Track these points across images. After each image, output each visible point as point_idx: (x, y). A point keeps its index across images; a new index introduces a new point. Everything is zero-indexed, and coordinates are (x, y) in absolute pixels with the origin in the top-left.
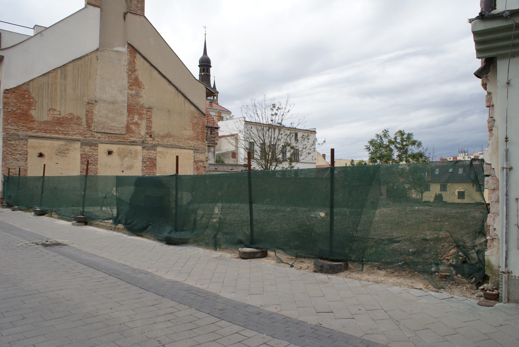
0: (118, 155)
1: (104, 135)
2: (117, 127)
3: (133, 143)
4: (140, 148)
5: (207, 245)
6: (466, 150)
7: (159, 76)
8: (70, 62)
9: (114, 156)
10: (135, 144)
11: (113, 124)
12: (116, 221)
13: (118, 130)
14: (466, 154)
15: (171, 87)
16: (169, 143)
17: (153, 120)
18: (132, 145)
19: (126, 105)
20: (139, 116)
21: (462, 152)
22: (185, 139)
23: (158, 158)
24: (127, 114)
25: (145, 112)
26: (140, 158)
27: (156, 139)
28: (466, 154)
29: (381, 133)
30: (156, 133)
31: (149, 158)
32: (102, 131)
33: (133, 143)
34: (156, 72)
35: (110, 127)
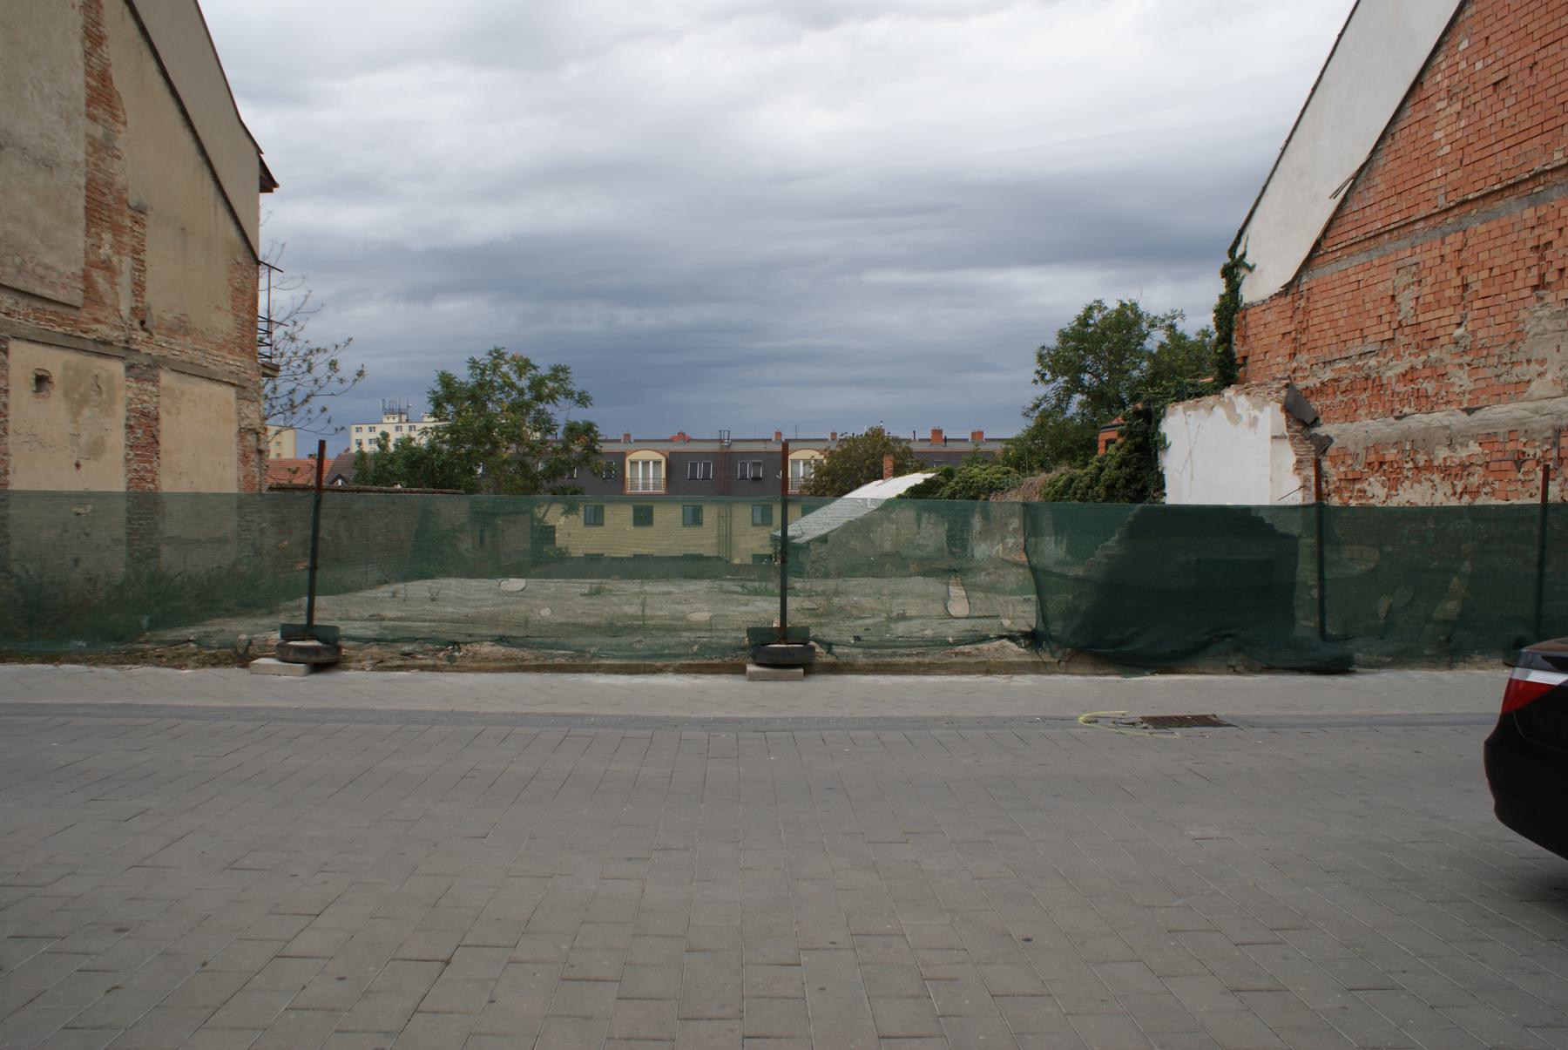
0: (66, 394)
1: (23, 302)
2: (61, 275)
3: (103, 349)
4: (117, 368)
5: (1433, 662)
6: (403, 407)
7: (159, 80)
8: (1375, 150)
9: (56, 399)
10: (107, 350)
11: (50, 259)
12: (1033, 639)
13: (64, 286)
14: (404, 417)
15: (185, 138)
16: (184, 357)
17: (149, 257)
18: (100, 354)
19: (82, 181)
20: (114, 236)
21: (391, 412)
22: (219, 348)
23: (163, 415)
24: (83, 223)
25: (128, 223)
26: (121, 411)
27: (157, 337)
28: (404, 417)
29: (483, 358)
30: (155, 312)
31: (143, 414)
32: (20, 284)
33: (103, 347)
34: (153, 65)
35: (40, 270)
